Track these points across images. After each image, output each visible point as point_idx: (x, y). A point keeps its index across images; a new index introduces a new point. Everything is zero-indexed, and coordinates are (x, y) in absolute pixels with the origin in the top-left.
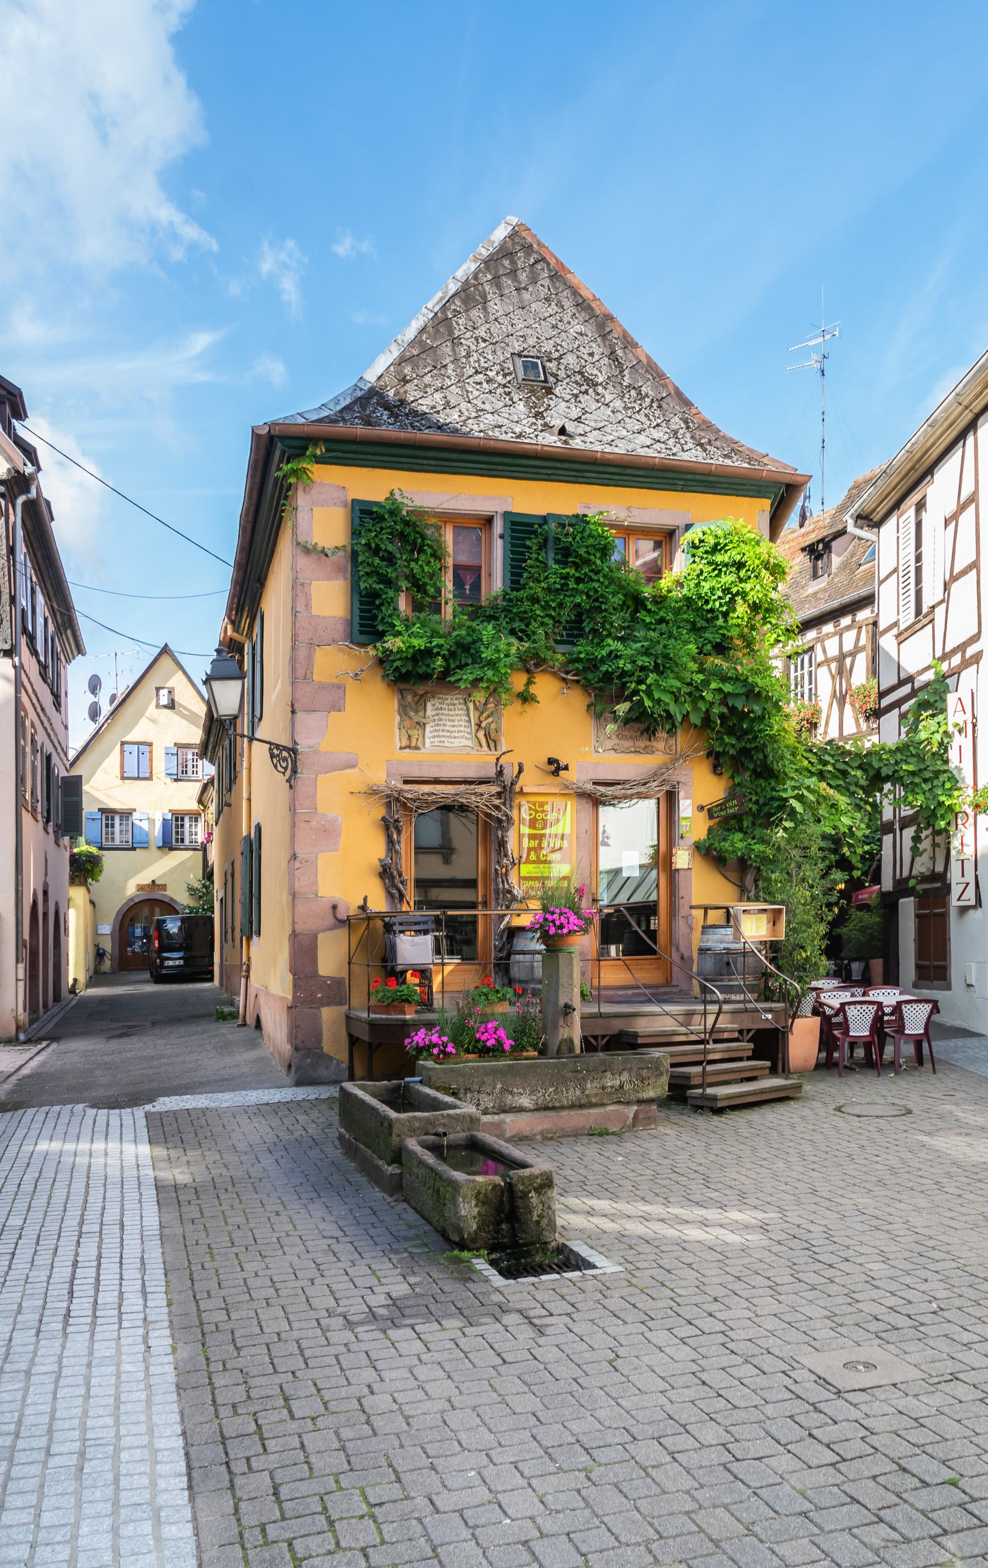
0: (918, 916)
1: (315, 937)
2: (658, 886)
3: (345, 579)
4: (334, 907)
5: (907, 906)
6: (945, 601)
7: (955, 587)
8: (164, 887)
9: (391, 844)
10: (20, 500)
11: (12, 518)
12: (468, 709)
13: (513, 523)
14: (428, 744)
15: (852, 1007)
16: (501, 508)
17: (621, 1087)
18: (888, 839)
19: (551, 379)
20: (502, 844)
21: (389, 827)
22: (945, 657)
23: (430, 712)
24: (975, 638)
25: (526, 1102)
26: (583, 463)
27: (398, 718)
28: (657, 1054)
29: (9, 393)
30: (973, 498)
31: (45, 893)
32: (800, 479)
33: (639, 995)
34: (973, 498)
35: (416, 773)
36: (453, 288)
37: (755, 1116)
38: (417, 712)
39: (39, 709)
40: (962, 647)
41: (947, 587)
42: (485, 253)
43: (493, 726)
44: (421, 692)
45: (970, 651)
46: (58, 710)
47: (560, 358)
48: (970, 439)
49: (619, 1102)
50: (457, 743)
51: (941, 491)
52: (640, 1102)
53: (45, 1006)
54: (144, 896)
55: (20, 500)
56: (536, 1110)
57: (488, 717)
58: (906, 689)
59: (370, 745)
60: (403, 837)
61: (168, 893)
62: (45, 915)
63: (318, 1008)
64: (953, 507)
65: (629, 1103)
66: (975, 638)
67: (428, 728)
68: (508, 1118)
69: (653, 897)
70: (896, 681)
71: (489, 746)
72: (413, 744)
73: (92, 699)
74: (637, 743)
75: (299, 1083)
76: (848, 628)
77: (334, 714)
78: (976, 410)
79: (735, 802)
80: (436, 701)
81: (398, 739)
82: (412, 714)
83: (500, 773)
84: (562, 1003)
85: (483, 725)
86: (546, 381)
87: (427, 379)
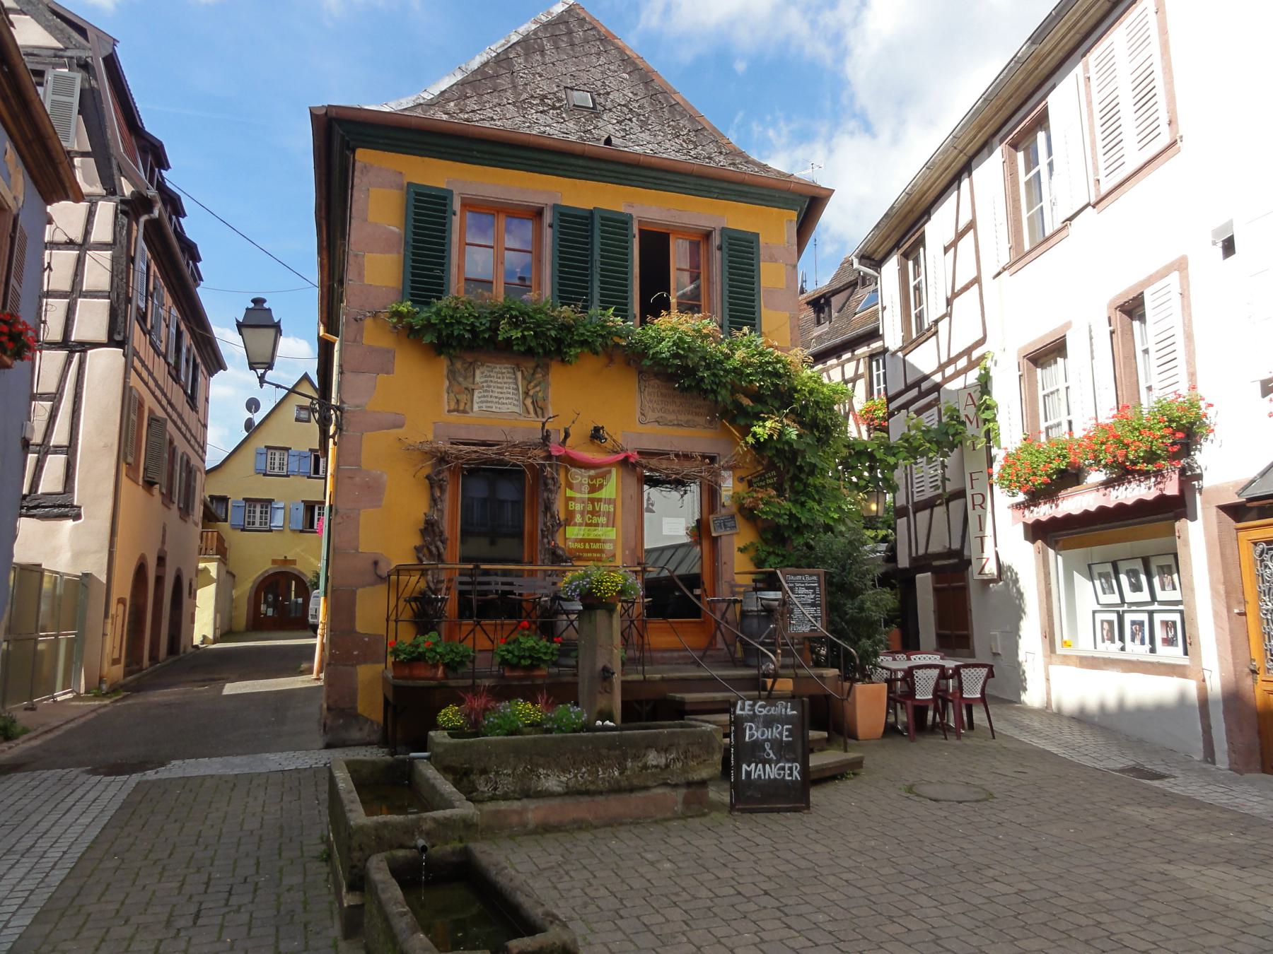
0: (935, 590)
1: (355, 593)
2: (701, 557)
3: (399, 253)
4: (376, 563)
5: (924, 581)
6: (948, 315)
7: (956, 302)
8: (294, 562)
9: (434, 501)
10: (143, 219)
11: (134, 233)
12: (516, 379)
13: (562, 214)
14: (476, 407)
15: (920, 672)
16: (551, 202)
17: (667, 766)
18: (902, 522)
19: (599, 107)
20: (548, 507)
21: (434, 483)
22: (951, 361)
23: (478, 379)
24: (982, 342)
25: (552, 783)
26: (627, 164)
27: (447, 383)
28: (710, 727)
29: (153, 145)
30: (972, 225)
31: (161, 560)
32: (823, 192)
33: (685, 657)
34: (972, 225)
35: (463, 435)
36: (514, 39)
37: (257, 330)
38: (465, 378)
39: (164, 402)
40: (968, 352)
41: (949, 302)
42: (544, 19)
43: (540, 394)
44: (470, 360)
45: (976, 354)
46: (194, 407)
47: (608, 93)
48: (965, 183)
49: (665, 784)
50: (504, 409)
51: (938, 228)
52: (689, 784)
53: (154, 658)
54: (277, 569)
55: (143, 219)
56: (566, 794)
57: (536, 386)
58: (914, 392)
59: (417, 405)
60: (447, 496)
61: (298, 567)
62: (159, 580)
63: (354, 666)
64: (952, 236)
65: (676, 786)
66: (982, 342)
67: (476, 394)
68: (531, 804)
69: (696, 570)
70: (903, 387)
71: (536, 413)
72: (461, 408)
73: (249, 415)
74: (680, 417)
75: (328, 746)
76: (849, 360)
77: (383, 376)
78: (970, 153)
79: (774, 473)
80: (484, 369)
81: (446, 402)
82: (461, 379)
83: (546, 438)
84: (599, 666)
85: (531, 393)
86: (594, 108)
87: (486, 97)
